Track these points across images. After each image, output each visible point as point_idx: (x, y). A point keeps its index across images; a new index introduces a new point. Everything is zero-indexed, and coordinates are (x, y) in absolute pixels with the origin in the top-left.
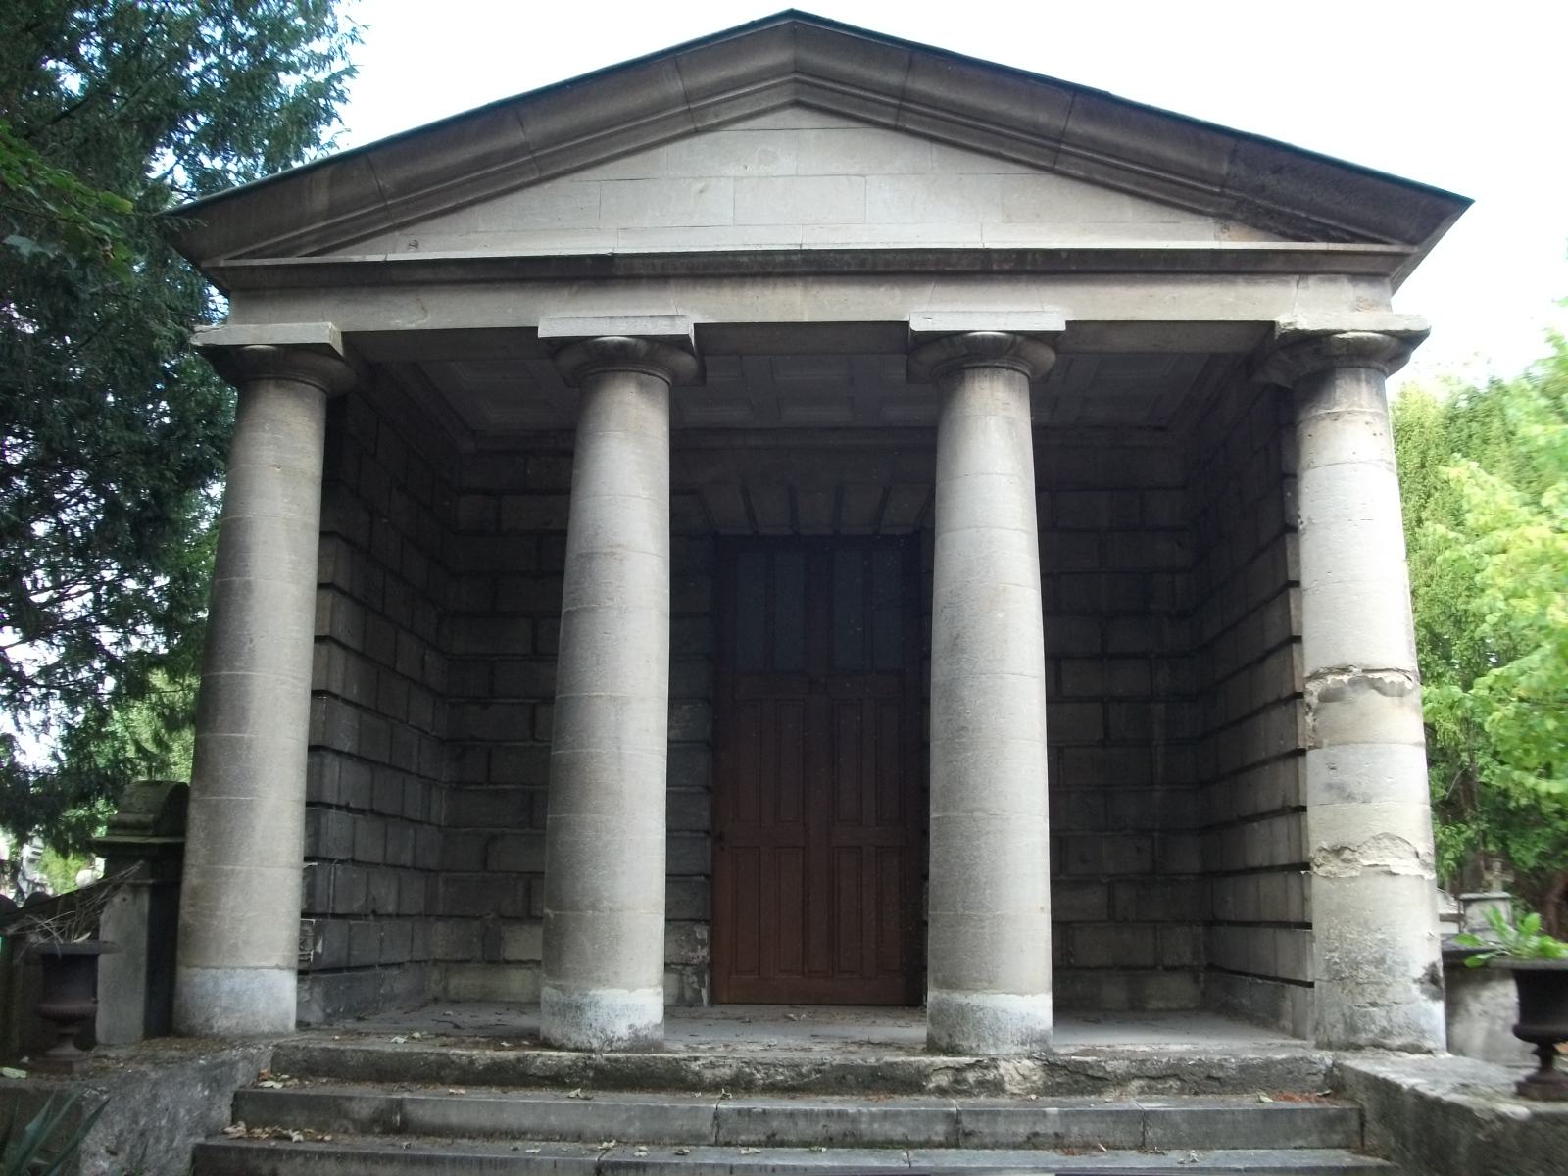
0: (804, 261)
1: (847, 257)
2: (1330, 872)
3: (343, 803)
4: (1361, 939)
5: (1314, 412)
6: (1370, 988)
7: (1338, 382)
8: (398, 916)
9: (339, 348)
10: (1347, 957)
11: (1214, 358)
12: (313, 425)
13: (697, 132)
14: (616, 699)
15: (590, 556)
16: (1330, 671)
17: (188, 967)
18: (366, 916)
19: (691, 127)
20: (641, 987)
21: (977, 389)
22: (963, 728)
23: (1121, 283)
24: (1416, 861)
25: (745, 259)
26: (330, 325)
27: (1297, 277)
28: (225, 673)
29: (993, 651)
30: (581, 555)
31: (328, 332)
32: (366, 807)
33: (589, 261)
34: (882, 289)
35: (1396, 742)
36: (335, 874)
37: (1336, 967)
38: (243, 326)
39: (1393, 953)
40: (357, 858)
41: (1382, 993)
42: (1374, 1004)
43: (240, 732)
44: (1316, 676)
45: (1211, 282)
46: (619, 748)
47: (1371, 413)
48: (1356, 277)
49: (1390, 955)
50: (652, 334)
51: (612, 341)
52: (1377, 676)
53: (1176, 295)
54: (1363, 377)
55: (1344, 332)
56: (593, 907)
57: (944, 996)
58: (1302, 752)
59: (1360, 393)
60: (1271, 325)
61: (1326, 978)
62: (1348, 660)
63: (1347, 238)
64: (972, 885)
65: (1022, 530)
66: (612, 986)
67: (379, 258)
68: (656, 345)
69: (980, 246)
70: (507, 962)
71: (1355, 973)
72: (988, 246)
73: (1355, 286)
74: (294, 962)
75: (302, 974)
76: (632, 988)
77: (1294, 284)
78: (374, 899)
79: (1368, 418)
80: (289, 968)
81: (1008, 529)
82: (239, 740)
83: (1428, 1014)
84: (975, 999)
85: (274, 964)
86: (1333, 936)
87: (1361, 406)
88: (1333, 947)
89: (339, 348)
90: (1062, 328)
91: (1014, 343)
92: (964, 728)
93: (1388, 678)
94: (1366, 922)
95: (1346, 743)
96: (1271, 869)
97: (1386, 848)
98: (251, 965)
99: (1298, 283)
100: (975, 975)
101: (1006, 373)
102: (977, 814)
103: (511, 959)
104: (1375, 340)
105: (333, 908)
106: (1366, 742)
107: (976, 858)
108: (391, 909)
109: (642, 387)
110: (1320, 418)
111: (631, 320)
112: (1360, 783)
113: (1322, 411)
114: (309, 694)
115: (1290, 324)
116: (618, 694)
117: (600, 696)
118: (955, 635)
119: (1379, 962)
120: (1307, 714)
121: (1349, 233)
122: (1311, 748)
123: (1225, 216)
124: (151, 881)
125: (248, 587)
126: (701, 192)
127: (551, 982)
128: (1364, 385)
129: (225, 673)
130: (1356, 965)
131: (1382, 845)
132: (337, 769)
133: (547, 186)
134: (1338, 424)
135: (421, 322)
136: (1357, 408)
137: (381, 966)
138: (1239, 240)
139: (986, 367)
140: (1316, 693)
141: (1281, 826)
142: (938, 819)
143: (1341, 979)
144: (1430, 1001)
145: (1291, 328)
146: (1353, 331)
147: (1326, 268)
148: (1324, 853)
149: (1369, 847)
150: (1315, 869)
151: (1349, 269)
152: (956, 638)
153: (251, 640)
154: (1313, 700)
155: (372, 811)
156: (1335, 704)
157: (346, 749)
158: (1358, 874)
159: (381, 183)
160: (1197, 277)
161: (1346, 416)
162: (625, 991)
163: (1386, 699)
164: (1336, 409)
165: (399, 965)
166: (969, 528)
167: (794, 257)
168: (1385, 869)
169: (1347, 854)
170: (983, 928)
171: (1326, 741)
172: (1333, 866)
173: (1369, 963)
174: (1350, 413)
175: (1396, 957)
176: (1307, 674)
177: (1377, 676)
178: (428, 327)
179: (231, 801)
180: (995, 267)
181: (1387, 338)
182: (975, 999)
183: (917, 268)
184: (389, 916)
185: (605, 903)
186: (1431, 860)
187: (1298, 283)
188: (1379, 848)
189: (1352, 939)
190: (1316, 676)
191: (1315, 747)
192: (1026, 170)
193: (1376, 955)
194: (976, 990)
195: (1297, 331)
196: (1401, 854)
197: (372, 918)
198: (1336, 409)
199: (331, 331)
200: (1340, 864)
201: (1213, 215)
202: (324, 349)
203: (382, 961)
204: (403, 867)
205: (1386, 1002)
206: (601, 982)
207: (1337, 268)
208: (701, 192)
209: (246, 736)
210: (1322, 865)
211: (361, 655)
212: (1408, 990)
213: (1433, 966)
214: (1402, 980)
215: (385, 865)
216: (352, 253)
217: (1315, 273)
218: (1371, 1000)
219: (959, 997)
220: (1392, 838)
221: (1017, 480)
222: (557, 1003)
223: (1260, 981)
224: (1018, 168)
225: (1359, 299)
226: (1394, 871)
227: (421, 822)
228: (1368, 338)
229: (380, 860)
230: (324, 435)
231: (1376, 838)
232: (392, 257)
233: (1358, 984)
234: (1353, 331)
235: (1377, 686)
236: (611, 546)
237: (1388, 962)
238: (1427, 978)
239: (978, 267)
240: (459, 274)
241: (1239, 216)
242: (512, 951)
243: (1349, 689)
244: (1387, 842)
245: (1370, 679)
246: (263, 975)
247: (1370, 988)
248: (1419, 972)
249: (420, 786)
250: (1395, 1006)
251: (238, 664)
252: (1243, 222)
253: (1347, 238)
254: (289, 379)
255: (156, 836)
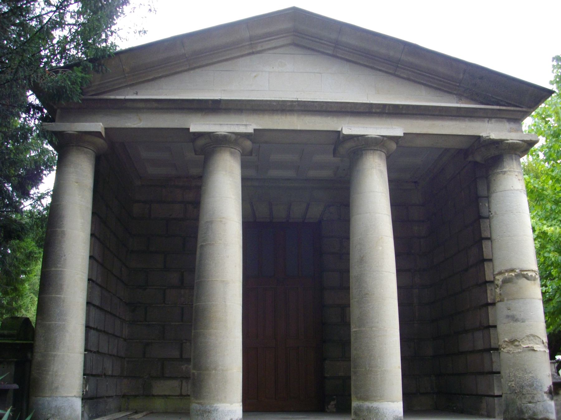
0: (298, 105)
1: (315, 104)
2: (510, 350)
3: (95, 327)
4: (523, 376)
5: (495, 171)
6: (528, 396)
7: (504, 160)
8: (112, 376)
9: (103, 134)
10: (518, 384)
11: (447, 150)
12: (91, 166)
13: (253, 53)
14: (224, 281)
15: (211, 222)
16: (507, 271)
17: (36, 397)
18: (102, 375)
19: (251, 51)
20: (235, 403)
21: (368, 158)
22: (367, 294)
23: (422, 119)
24: (542, 345)
25: (275, 104)
26: (101, 124)
27: (488, 119)
28: (53, 269)
29: (378, 262)
30: (207, 222)
31: (100, 127)
32: (103, 329)
33: (210, 102)
34: (329, 118)
35: (534, 298)
36: (93, 358)
37: (514, 388)
38: (62, 123)
39: (536, 382)
40: (100, 351)
41: (533, 397)
42: (530, 402)
43: (60, 294)
44: (500, 273)
45: (456, 120)
46: (225, 302)
47: (518, 172)
48: (510, 120)
49: (535, 383)
50: (238, 131)
51: (221, 134)
52: (525, 273)
53: (443, 124)
54: (514, 158)
55: (508, 140)
56: (215, 369)
57: (361, 403)
58: (493, 304)
59: (513, 164)
60: (479, 137)
61: (509, 392)
62: (514, 267)
63: (506, 105)
64: (373, 358)
65: (387, 215)
66: (224, 402)
67: (122, 97)
68: (239, 137)
69: (368, 102)
70: (153, 396)
71: (522, 390)
72: (371, 102)
73: (509, 123)
74: (81, 395)
75: (82, 399)
76: (231, 403)
77: (487, 121)
78: (105, 368)
79: (516, 174)
80: (79, 397)
81: (382, 214)
82: (59, 298)
83: (550, 405)
84: (375, 404)
85: (73, 395)
86: (511, 376)
87: (514, 169)
88: (512, 380)
89: (103, 134)
90: (402, 135)
91: (383, 140)
92: (367, 294)
93: (530, 274)
94: (526, 369)
95: (514, 299)
96: (473, 352)
97: (532, 340)
98: (64, 395)
99: (488, 121)
100: (374, 395)
101: (379, 152)
102: (374, 329)
103: (156, 394)
104: (519, 143)
105: (92, 372)
106: (522, 299)
107: (373, 346)
108: (110, 373)
109: (232, 154)
110: (498, 173)
111: (229, 126)
112: (520, 315)
113: (499, 171)
114: (87, 280)
115: (487, 136)
116: (224, 280)
117: (217, 280)
118: (362, 256)
119: (531, 385)
120: (496, 288)
121: (507, 103)
122: (498, 301)
123: (460, 96)
124: (16, 360)
125: (63, 233)
126: (255, 76)
127: (196, 401)
128: (514, 161)
129: (53, 269)
130: (522, 387)
131: (530, 339)
132: (94, 312)
133: (192, 72)
134: (506, 176)
135: (139, 124)
136: (512, 170)
137: (107, 397)
138: (466, 103)
139: (371, 150)
140: (501, 280)
141: (479, 335)
142: (355, 331)
143: (516, 393)
144: (550, 400)
145: (488, 138)
146: (512, 140)
147: (498, 116)
148: (506, 343)
149: (525, 340)
150: (502, 349)
151: (508, 117)
152: (362, 258)
153: (65, 255)
154: (499, 283)
155: (104, 331)
156: (509, 284)
157: (97, 304)
158: (521, 351)
159: (124, 67)
160: (451, 117)
161: (508, 172)
162: (229, 405)
163: (529, 282)
164: (504, 170)
165: (112, 397)
166: (367, 213)
167: (294, 104)
168: (532, 348)
169: (517, 343)
170: (377, 375)
171: (506, 299)
172: (511, 348)
173: (528, 386)
174: (509, 171)
175: (537, 383)
176: (496, 272)
177: (525, 273)
178: (141, 126)
179: (56, 324)
180: (374, 111)
181: (523, 143)
182: (375, 404)
183: (343, 110)
184: (109, 376)
185: (220, 367)
186: (547, 345)
187: (488, 121)
188: (529, 340)
189: (520, 377)
190: (500, 273)
191: (501, 301)
192: (384, 74)
193: (530, 383)
194: (375, 401)
195: (490, 139)
196: (537, 342)
197: (103, 377)
198: (504, 170)
199: (101, 126)
200: (513, 347)
201: (456, 94)
202: (98, 134)
203: (107, 395)
204: (114, 356)
205: (534, 401)
206: (219, 401)
207: (503, 116)
208: (255, 76)
209: (62, 296)
210: (505, 348)
211: (102, 265)
212: (543, 396)
213: (550, 386)
214: (540, 392)
215: (108, 354)
216: (112, 95)
217: (494, 118)
218: (529, 400)
219: (367, 404)
220: (534, 336)
221: (384, 194)
222: (199, 410)
223: (468, 397)
224: (381, 73)
225: (511, 128)
226: (535, 349)
227: (119, 337)
228: (517, 143)
229: (107, 352)
230: (94, 171)
231: (528, 336)
232: (127, 97)
233: (523, 394)
234: (512, 140)
235: (527, 278)
236: (220, 218)
237: (535, 385)
238: (548, 391)
239: (367, 110)
240: (155, 105)
241: (465, 95)
242: (155, 391)
243: (515, 278)
244: (532, 338)
245: (523, 275)
246: (69, 400)
247: (528, 396)
248: (546, 389)
249: (119, 322)
250: (538, 403)
251: (59, 266)
252: (467, 98)
253: (506, 105)
254: (81, 146)
255: (18, 340)
